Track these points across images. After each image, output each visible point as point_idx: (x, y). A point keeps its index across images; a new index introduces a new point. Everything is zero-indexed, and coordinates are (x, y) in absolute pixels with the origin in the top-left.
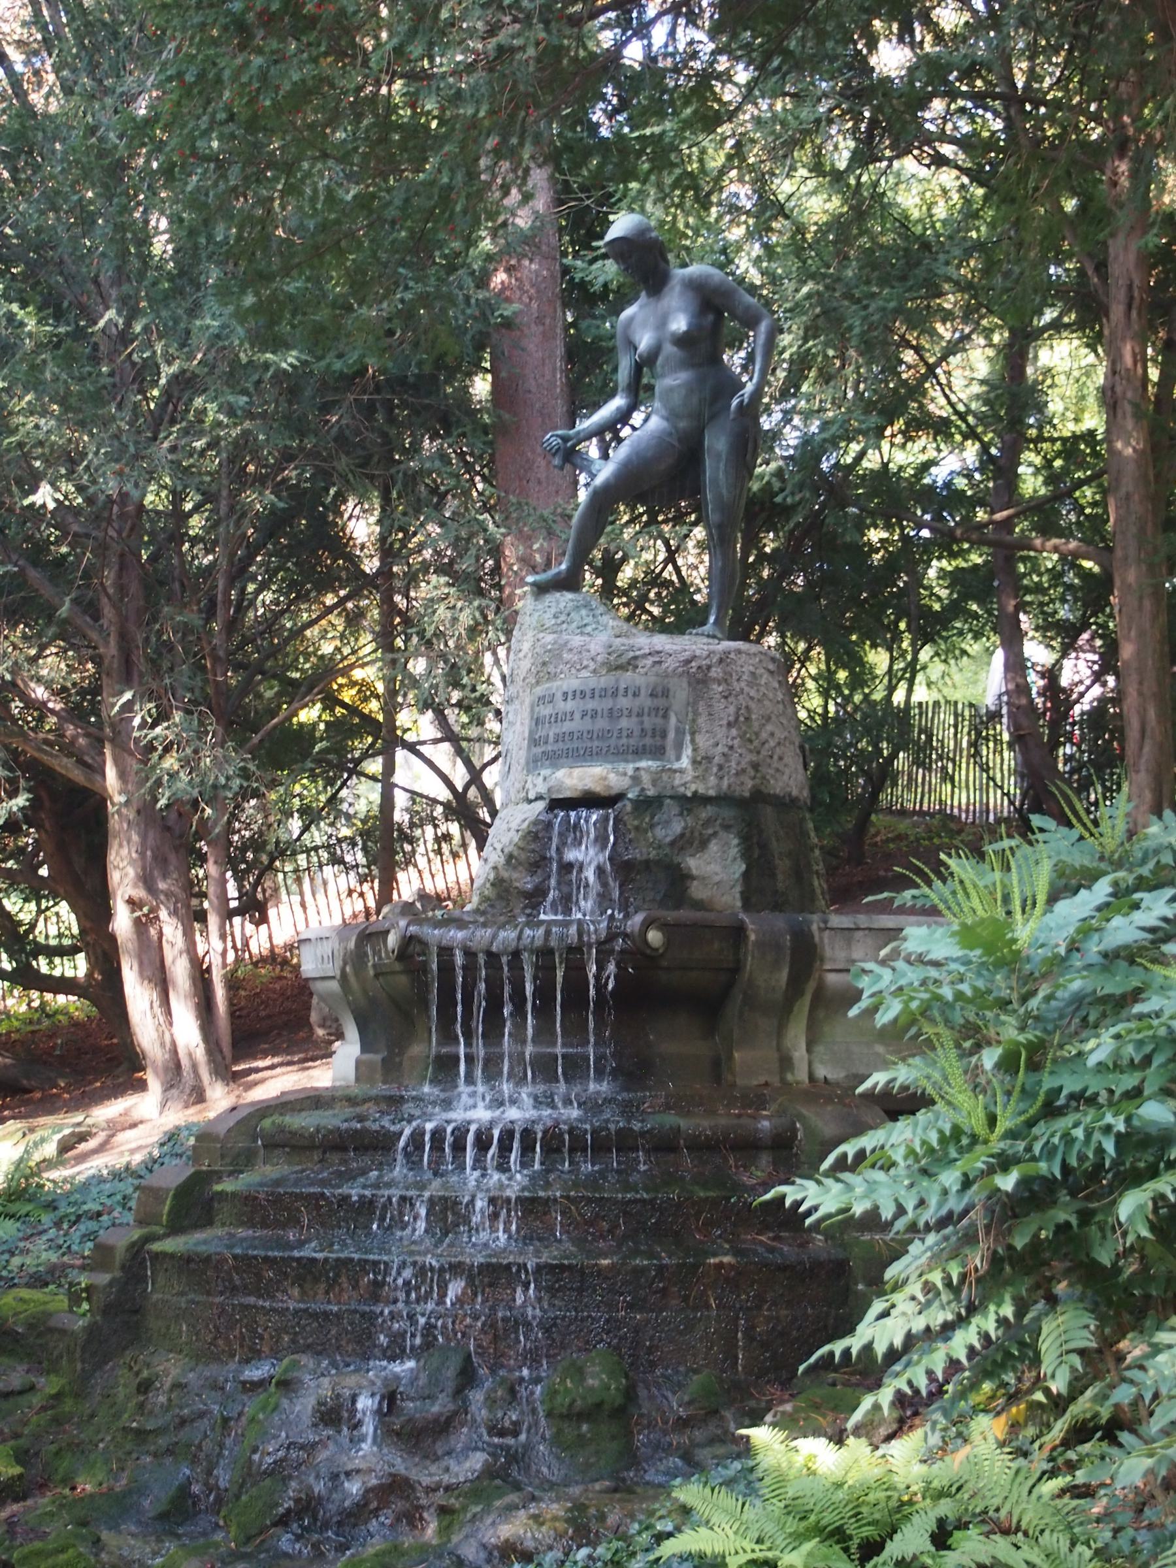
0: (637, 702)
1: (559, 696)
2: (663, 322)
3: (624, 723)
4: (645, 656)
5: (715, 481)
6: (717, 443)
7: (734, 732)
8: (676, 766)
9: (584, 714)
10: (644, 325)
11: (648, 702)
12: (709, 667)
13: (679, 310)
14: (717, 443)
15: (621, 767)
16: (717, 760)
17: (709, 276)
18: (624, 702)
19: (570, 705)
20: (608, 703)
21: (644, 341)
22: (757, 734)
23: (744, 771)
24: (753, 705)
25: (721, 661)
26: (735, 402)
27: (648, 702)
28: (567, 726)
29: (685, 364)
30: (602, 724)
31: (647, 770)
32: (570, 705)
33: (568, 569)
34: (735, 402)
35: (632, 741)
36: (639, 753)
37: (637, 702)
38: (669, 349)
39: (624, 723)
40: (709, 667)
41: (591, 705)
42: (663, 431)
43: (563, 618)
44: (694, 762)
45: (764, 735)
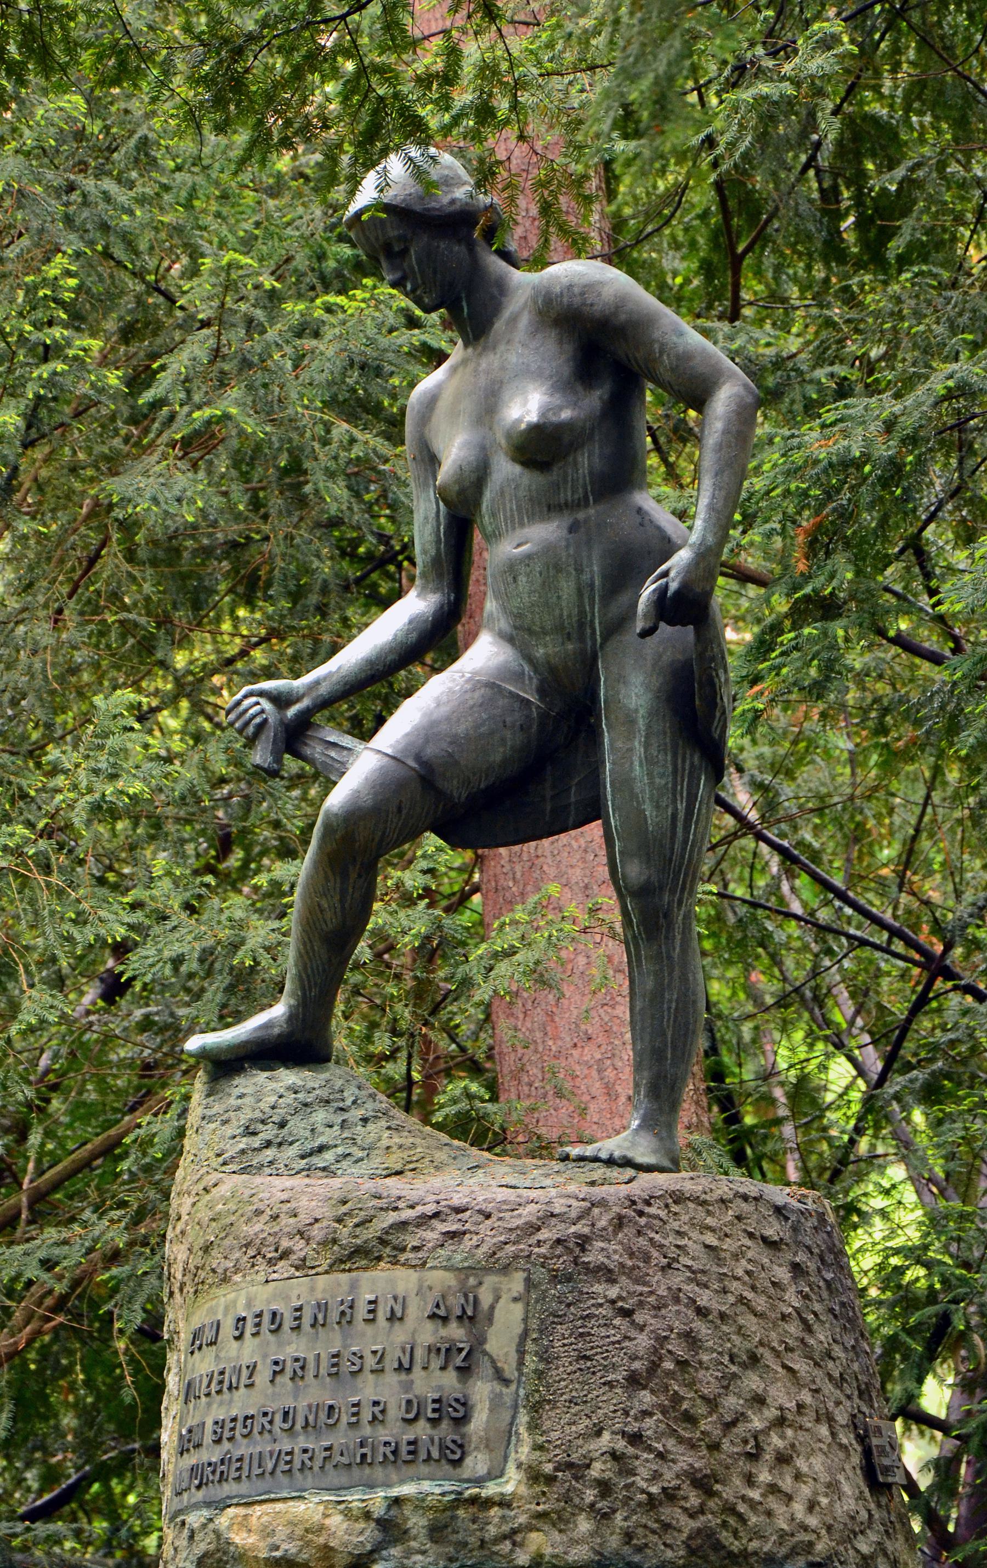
0: (400, 1335)
1: (228, 1329)
2: (488, 405)
3: (368, 1389)
4: (424, 1220)
5: (624, 783)
6: (632, 689)
7: (646, 1398)
8: (491, 1490)
9: (278, 1369)
10: (454, 414)
11: (428, 1334)
12: (583, 1242)
13: (538, 375)
14: (632, 689)
15: (355, 1498)
16: (596, 1470)
17: (590, 287)
18: (370, 1340)
19: (248, 1351)
20: (331, 1341)
21: (454, 450)
22: (712, 1403)
23: (670, 1495)
24: (702, 1328)
25: (620, 1222)
26: (648, 591)
27: (428, 1334)
28: (241, 1403)
29: (547, 506)
30: (316, 1393)
31: (419, 1503)
32: (248, 1351)
33: (292, 1017)
34: (648, 591)
35: (384, 1434)
36: (404, 1457)
37: (400, 1335)
38: (505, 469)
39: (368, 1389)
40: (583, 1242)
41: (294, 1347)
42: (506, 673)
43: (269, 1132)
44: (534, 1476)
45: (732, 1402)
